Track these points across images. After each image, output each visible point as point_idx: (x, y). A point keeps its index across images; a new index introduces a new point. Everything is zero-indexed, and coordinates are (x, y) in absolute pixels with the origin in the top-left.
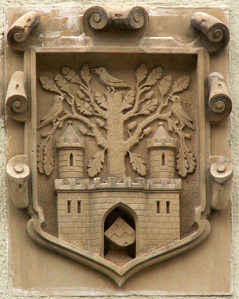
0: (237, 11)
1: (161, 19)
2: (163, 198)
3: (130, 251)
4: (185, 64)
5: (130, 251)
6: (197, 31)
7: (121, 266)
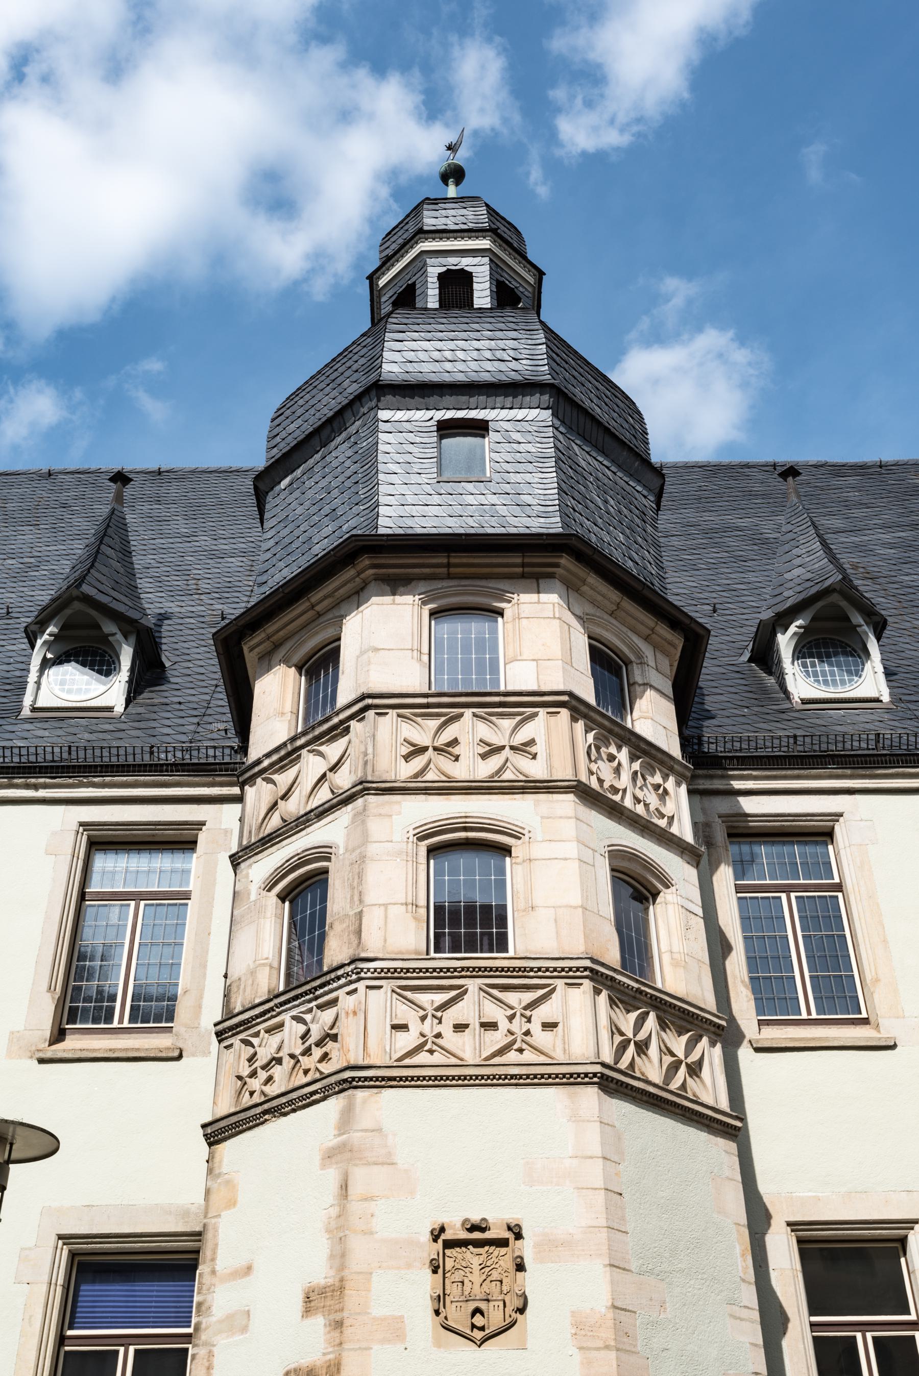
2: (496, 1303)
3: (482, 1329)
4: (502, 1243)
5: (482, 1329)
7: (478, 1335)
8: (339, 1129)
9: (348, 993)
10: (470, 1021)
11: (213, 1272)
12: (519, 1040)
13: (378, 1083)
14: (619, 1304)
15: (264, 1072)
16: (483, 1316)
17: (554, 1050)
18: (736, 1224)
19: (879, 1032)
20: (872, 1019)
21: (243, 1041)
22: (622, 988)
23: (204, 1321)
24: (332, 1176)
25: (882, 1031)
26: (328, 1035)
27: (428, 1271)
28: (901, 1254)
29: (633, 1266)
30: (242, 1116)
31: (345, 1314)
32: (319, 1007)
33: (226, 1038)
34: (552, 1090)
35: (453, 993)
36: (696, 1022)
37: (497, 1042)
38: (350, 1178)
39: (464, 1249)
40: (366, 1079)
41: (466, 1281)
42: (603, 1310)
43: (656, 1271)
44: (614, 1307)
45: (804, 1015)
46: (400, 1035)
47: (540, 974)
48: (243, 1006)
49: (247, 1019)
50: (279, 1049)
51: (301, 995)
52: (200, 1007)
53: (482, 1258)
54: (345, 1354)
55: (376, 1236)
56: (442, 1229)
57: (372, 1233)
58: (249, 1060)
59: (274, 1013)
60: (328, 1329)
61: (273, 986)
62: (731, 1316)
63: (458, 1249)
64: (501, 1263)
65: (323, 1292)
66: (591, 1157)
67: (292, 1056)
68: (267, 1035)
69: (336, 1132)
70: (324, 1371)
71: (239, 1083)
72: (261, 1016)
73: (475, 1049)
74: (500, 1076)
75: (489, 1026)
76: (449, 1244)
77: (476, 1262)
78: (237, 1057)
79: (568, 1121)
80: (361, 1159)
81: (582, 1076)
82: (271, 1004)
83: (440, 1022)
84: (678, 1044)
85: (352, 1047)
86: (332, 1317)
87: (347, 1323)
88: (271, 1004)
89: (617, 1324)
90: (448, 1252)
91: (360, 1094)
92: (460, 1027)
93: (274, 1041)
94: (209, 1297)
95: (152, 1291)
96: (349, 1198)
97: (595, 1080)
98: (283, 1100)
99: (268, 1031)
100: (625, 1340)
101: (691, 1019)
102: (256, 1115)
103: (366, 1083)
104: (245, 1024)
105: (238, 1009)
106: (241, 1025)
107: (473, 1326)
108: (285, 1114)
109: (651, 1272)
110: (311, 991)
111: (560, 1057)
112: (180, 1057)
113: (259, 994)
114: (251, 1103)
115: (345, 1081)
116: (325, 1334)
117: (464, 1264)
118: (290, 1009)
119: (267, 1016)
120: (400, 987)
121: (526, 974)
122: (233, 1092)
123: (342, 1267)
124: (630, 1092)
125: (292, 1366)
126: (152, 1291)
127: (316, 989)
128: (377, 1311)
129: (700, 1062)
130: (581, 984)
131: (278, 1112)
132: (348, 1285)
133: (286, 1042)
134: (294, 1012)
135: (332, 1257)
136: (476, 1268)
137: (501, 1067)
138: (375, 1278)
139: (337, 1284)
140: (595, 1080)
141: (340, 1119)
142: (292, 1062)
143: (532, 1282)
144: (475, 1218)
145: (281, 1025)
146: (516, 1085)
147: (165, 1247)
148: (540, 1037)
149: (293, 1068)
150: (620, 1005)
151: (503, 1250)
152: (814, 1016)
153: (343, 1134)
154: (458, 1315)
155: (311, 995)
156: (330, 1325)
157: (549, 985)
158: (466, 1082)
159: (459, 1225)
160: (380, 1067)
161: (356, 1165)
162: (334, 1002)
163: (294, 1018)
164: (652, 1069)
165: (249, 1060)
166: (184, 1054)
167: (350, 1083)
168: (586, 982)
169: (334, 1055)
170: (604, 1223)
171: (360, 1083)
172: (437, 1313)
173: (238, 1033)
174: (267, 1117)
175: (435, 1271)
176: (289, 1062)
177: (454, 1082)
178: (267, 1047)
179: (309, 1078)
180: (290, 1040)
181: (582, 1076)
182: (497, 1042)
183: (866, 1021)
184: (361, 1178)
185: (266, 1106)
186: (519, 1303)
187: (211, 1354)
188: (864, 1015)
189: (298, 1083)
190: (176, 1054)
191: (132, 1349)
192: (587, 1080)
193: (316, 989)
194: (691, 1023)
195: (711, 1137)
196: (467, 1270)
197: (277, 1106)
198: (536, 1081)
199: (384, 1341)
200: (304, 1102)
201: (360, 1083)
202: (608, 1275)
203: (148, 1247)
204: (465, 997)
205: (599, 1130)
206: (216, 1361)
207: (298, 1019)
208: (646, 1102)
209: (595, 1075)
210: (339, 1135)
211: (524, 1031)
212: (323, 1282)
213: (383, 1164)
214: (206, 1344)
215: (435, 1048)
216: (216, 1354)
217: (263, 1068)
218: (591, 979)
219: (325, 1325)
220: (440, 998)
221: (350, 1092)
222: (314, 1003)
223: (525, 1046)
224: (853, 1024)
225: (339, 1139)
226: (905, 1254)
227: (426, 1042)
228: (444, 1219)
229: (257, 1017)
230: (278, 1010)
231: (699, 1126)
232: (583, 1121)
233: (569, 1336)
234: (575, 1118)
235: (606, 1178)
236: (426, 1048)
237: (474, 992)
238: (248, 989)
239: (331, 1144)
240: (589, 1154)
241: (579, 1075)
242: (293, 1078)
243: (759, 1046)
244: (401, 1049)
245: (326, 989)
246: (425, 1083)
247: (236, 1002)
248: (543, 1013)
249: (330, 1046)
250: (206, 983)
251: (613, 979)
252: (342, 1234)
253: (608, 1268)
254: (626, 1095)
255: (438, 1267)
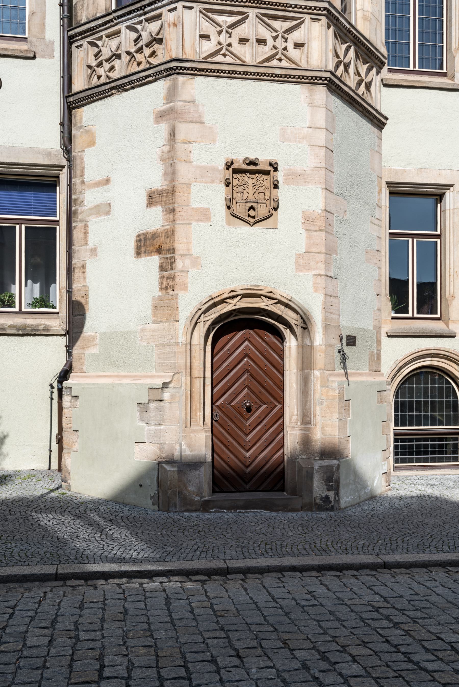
0: (155, 673)
1: (262, 162)
2: (262, 205)
3: (254, 217)
4: (267, 173)
5: (254, 217)
6: (271, 165)
7: (252, 220)
8: (167, 100)
9: (170, 11)
10: (250, 37)
11: (83, 183)
12: (280, 52)
13: (192, 72)
14: (328, 209)
15: (107, 64)
16: (255, 210)
17: (301, 62)
18: (378, 176)
19: (454, 81)
20: (449, 74)
21: (89, 43)
22: (341, 27)
23: (80, 209)
24: (163, 129)
25: (455, 80)
26: (155, 39)
27: (224, 186)
28: (439, 202)
29: (335, 191)
30: (96, 90)
31: (176, 205)
32: (147, 20)
33: (77, 40)
34: (298, 86)
35: (239, 17)
36: (372, 58)
37: (266, 53)
38: (176, 129)
39: (244, 175)
40: (185, 68)
41: (245, 192)
42: (320, 211)
43: (344, 195)
44: (326, 210)
45: (411, 68)
46: (205, 43)
47: (296, 9)
48: (87, 18)
49: (93, 27)
50: (118, 48)
51: (134, 11)
52: (44, 25)
53: (254, 180)
54: (176, 226)
55: (193, 164)
56: (232, 163)
57: (190, 162)
58: (96, 56)
59: (113, 24)
60: (165, 213)
61: (108, 6)
62: (371, 222)
63: (240, 175)
64: (265, 183)
65: (160, 193)
66: (319, 128)
67: (128, 53)
68: (107, 39)
69: (165, 102)
70: (163, 235)
71: (89, 71)
72: (103, 26)
73: (253, 56)
74: (269, 74)
75: (261, 42)
76: (236, 171)
77: (250, 182)
78: (86, 53)
79: (308, 106)
80: (182, 118)
81: (318, 78)
82: (111, 17)
83: (230, 37)
84: (363, 69)
85: (173, 47)
86: (167, 207)
87: (177, 210)
88: (111, 17)
89: (326, 219)
90: (235, 176)
91: (181, 79)
92: (243, 41)
93: (114, 43)
94: (82, 197)
95: (31, 197)
96: (176, 141)
97: (326, 82)
98: (126, 80)
99: (108, 36)
100: (329, 227)
101: (370, 55)
102: (105, 90)
103: (185, 71)
104: (91, 31)
105: (84, 20)
106: (88, 32)
107: (249, 216)
108: (126, 90)
109: (341, 195)
110: (141, 8)
111: (304, 65)
112: (34, 58)
113: (99, 11)
114: (98, 83)
115: (171, 69)
116: (163, 216)
117: (244, 183)
118: (125, 21)
119: (107, 26)
120: (205, 9)
121: (287, 8)
122: (86, 76)
123: (173, 180)
124: (341, 93)
125: (142, 232)
126: (31, 197)
127: (145, 6)
128: (194, 205)
129: (370, 83)
130: (320, 20)
131: (122, 88)
132: (178, 190)
133: (123, 43)
134: (128, 23)
135: (165, 174)
136: (250, 185)
137: (270, 69)
138: (192, 187)
139: (170, 189)
140: (326, 82)
141: (168, 93)
142: (128, 57)
143: (282, 194)
144: (252, 157)
145: (118, 33)
146: (278, 81)
147: (38, 173)
148: (293, 53)
149: (130, 61)
150: (339, 38)
151: (266, 177)
152: (417, 69)
153: (171, 102)
154: (241, 210)
155: (142, 11)
156: (166, 211)
157: (301, 18)
158: (247, 76)
159: (241, 161)
160: (194, 61)
161: (180, 122)
162: (159, 17)
163: (127, 27)
164: (351, 81)
165: (96, 56)
166: (37, 56)
167: (175, 70)
168: (324, 18)
169: (159, 53)
170: (323, 165)
171: (181, 71)
172: (229, 207)
173: (85, 37)
174: (113, 91)
175: (227, 185)
176: (126, 57)
177: (240, 76)
178: (108, 47)
179: (142, 67)
180: (126, 42)
181: (318, 78)
182: (266, 53)
183: (445, 75)
184: (183, 130)
185: (113, 85)
186: (273, 205)
187: (86, 226)
188: (445, 71)
189: (133, 71)
190: (32, 55)
191: (23, 226)
192: (321, 81)
193: (145, 6)
194: (370, 58)
195: (372, 127)
196: (245, 186)
197: (121, 85)
198: (290, 79)
199: (198, 220)
200: (140, 82)
201: (181, 71)
202: (324, 193)
203: (27, 172)
204: (247, 21)
205: (325, 113)
206: (90, 230)
207: (131, 28)
208: (347, 101)
209: (326, 78)
210: (167, 103)
211: (283, 47)
212: (160, 188)
213: (196, 122)
214: (82, 221)
215: (227, 53)
216: (89, 226)
217: (107, 61)
218: (327, 17)
219: (163, 211)
220: (231, 20)
221: (175, 76)
222: (143, 17)
223: (283, 57)
224: (438, 75)
225: (168, 106)
226: (441, 202)
227: (221, 49)
228: (233, 157)
229: (100, 26)
230: (115, 21)
231: (368, 120)
232: (316, 107)
233: (301, 223)
234: (312, 104)
235: (327, 141)
236: (222, 53)
237: (253, 17)
238: (91, 7)
239: (161, 109)
240: (318, 126)
241: (316, 78)
242: (129, 68)
243: (387, 83)
244: (205, 52)
245: (153, 7)
246: (222, 74)
247: (81, 16)
248: (296, 36)
249: (156, 47)
250: (47, 8)
251: (338, 19)
252: (172, 162)
253: (324, 190)
254: (338, 94)
255: (230, 183)
